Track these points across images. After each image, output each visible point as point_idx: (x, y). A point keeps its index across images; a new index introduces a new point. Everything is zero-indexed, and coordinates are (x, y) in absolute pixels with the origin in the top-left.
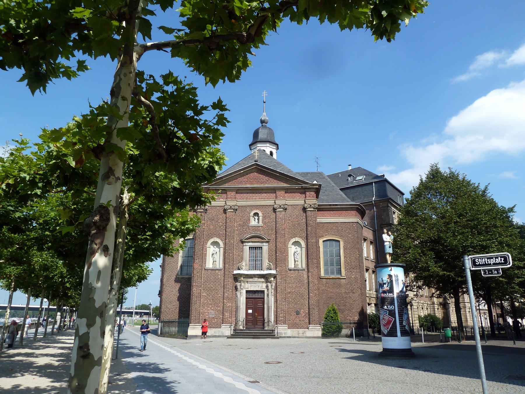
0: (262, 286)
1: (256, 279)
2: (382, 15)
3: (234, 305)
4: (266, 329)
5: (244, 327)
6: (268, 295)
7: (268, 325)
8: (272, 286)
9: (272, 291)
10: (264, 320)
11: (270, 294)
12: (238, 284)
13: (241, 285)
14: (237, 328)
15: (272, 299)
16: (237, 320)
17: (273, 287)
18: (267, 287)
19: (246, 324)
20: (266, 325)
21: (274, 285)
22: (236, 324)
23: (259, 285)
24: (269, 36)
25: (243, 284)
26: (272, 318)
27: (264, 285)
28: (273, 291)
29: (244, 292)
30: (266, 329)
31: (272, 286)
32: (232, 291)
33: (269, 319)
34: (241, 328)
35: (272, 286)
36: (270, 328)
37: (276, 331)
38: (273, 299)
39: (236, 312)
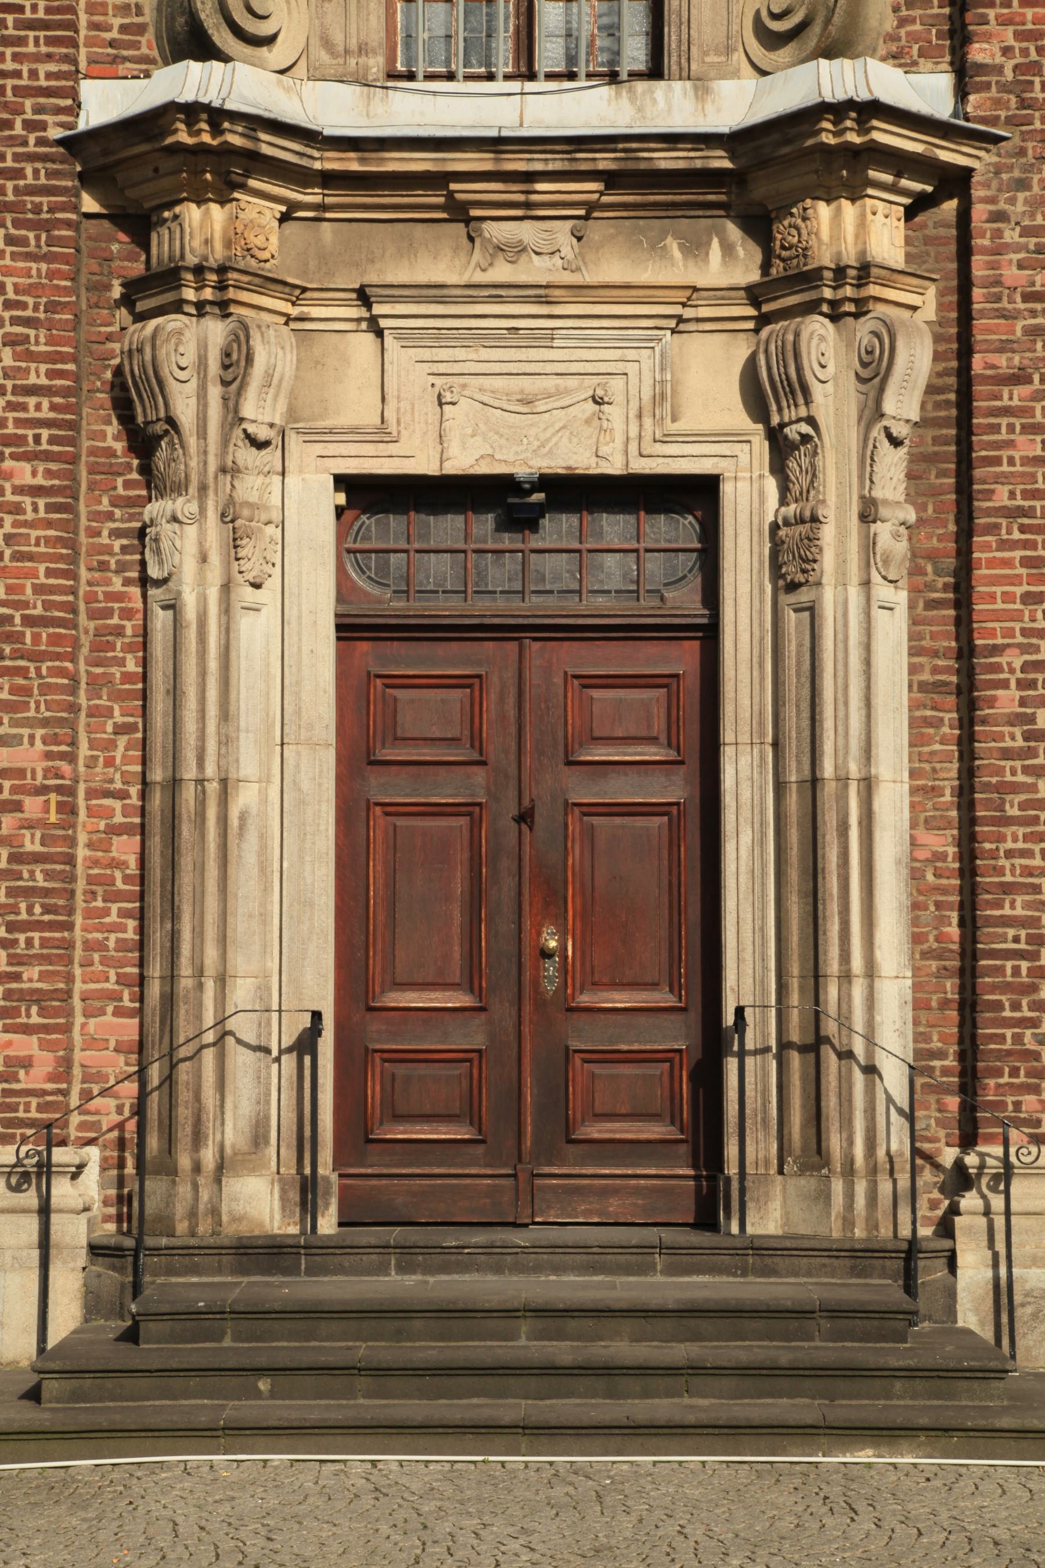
0: (664, 399)
1: (544, 249)
2: (260, 1391)
3: (106, 761)
4: (769, 1217)
5: (307, 1194)
6: (791, 563)
7: (810, 1153)
8: (869, 400)
9: (868, 481)
10: (715, 1040)
11: (836, 542)
12: (186, 344)
13: (235, 365)
14: (175, 1200)
15: (876, 636)
16: (161, 1052)
17: (904, 404)
18: (770, 394)
19: (356, 1135)
20: (752, 1149)
21: (916, 361)
22: (152, 1141)
23: (605, 370)
24: (841, 96)
25: (273, 353)
26: (888, 1007)
27: (711, 374)
28: (892, 468)
29: (304, 504)
30: (769, 1217)
31: (874, 372)
32: (63, 500)
33: (812, 1045)
34: (258, 1203)
35: (874, 372)
36: (856, 1208)
37: (973, 1270)
38: (892, 632)
39: (157, 895)
